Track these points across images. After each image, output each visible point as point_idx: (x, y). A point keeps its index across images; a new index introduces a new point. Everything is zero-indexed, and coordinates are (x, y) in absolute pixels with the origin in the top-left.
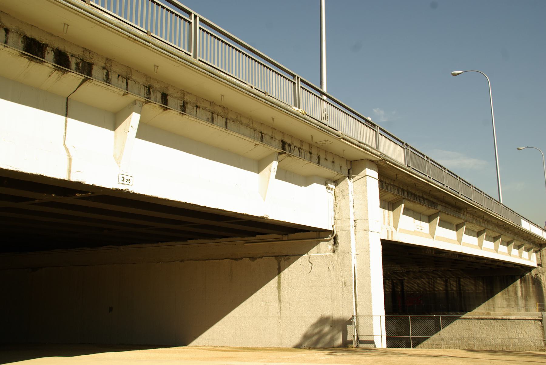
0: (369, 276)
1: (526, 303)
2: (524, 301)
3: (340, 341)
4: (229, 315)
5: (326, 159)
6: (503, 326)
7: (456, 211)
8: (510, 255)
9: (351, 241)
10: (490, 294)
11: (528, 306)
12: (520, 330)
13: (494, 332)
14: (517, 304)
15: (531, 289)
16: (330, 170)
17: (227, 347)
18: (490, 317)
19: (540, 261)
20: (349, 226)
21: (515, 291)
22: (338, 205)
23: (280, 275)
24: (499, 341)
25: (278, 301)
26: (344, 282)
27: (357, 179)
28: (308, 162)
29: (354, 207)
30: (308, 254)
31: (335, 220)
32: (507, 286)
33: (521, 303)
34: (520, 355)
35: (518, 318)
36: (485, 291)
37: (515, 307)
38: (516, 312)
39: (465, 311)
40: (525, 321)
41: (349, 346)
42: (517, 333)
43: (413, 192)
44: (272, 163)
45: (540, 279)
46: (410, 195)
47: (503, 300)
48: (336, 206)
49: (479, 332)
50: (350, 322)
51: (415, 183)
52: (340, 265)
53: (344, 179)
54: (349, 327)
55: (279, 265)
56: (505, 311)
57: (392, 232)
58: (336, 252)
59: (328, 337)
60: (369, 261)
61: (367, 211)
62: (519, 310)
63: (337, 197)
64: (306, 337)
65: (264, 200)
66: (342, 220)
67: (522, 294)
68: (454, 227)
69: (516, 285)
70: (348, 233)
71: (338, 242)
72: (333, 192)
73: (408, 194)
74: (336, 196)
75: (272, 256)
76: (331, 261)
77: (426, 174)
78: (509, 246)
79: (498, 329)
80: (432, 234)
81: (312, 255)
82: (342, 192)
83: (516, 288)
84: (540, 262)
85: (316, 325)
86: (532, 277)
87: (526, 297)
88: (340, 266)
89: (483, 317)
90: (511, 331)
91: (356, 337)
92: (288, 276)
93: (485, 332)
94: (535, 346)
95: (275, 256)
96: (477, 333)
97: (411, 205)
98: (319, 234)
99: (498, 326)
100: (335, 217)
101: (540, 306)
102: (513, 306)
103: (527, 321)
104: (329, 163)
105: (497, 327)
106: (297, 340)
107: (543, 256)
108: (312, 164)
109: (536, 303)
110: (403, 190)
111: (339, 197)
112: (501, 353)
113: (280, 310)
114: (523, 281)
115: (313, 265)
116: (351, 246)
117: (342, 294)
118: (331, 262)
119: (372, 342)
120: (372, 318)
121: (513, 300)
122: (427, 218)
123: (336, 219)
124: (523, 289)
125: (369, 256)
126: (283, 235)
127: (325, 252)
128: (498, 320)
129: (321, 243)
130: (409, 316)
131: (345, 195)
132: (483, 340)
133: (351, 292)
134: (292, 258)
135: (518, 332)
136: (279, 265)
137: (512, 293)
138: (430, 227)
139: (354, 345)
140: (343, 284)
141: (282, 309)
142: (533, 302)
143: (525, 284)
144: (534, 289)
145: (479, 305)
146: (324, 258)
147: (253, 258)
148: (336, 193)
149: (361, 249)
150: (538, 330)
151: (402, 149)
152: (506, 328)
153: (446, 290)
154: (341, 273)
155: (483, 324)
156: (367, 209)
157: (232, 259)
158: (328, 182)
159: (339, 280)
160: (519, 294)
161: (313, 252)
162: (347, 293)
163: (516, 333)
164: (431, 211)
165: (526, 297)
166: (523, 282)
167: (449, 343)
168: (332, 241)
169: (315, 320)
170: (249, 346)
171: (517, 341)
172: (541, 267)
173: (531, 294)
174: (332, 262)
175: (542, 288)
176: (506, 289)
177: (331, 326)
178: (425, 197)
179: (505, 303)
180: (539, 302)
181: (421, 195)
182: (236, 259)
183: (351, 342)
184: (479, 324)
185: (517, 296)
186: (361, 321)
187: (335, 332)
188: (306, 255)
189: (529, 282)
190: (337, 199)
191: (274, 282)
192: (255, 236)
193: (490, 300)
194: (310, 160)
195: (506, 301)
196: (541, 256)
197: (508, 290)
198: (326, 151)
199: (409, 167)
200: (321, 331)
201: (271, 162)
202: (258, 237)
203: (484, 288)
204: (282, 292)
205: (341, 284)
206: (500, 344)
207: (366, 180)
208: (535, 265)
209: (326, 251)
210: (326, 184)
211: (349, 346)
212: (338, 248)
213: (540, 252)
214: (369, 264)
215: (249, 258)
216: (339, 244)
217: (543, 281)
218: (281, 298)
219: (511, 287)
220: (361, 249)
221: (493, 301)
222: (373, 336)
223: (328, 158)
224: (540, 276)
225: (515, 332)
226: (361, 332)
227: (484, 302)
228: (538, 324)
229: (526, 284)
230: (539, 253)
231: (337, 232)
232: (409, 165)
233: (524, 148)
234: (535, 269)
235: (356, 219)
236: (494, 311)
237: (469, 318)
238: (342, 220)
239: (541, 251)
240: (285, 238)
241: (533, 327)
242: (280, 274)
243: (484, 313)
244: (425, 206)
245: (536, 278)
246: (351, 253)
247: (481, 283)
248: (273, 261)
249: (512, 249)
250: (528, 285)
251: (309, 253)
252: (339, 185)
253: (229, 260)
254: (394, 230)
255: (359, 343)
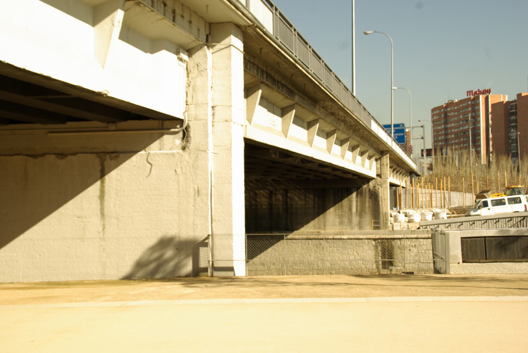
0: (230, 183)
1: (360, 219)
2: (358, 218)
3: (189, 268)
4: (22, 237)
5: (182, 16)
6: (334, 247)
7: (312, 105)
8: (354, 163)
9: (208, 134)
10: (321, 210)
11: (363, 223)
12: (351, 251)
13: (324, 254)
14: (350, 221)
15: (367, 204)
16: (186, 33)
17: (18, 283)
18: (320, 237)
19: (380, 171)
20: (207, 114)
21: (349, 206)
22: (192, 84)
23: (104, 180)
24: (328, 264)
25: (100, 215)
26: (196, 189)
27: (218, 50)
28: (161, 17)
29: (212, 88)
30: (145, 151)
31: (187, 104)
32: (341, 199)
33: (355, 219)
34: (482, 280)
35: (351, 237)
36: (316, 206)
37: (348, 224)
38: (349, 231)
39: (291, 229)
40: (358, 240)
41: (202, 275)
42: (348, 254)
43: (273, 75)
44: (116, 12)
45: (378, 191)
46: (269, 79)
47: (336, 216)
48: (189, 86)
49: (307, 255)
50: (204, 243)
51: (278, 63)
52: (191, 166)
53: (200, 47)
54: (202, 250)
55: (102, 165)
56: (337, 229)
57: (246, 126)
58: (187, 149)
59: (172, 264)
60: (231, 162)
61: (231, 94)
62: (352, 228)
63: (190, 73)
64: (140, 265)
65: (103, 67)
66: (197, 105)
67: (357, 209)
68: (306, 125)
69: (352, 199)
70: (204, 123)
71: (190, 135)
72: (184, 65)
73: (267, 77)
74: (189, 71)
75: (92, 153)
76: (180, 162)
77: (293, 51)
78: (355, 152)
79: (328, 250)
80: (285, 132)
81: (152, 152)
82: (198, 66)
83: (350, 203)
84: (379, 173)
85: (153, 249)
86: (370, 189)
87: (361, 213)
88: (192, 168)
89: (312, 237)
90: (342, 253)
91: (211, 263)
92: (116, 180)
93: (313, 254)
94: (367, 269)
95: (97, 153)
96: (303, 256)
97: (268, 91)
98: (163, 123)
99: (328, 247)
100: (187, 101)
101: (375, 223)
102: (346, 224)
103: (360, 240)
104: (186, 23)
105: (327, 248)
106: (126, 268)
107: (383, 165)
108: (165, 21)
109: (372, 220)
110: (262, 71)
111: (193, 74)
112: (258, 278)
113: (104, 229)
114: (360, 194)
115: (153, 166)
116: (208, 141)
117: (193, 206)
118: (179, 163)
119: (231, 269)
120: (232, 238)
121: (347, 216)
122: (279, 111)
123: (188, 103)
124: (359, 204)
125: (231, 156)
126: (108, 122)
127: (171, 149)
128: (328, 240)
129: (166, 137)
130: (283, 235)
131: (202, 71)
132: (310, 263)
133: (207, 204)
134: (122, 155)
135: (349, 253)
136: (102, 165)
137: (346, 209)
138: (283, 123)
139: (209, 273)
140: (195, 193)
141: (106, 226)
142: (368, 219)
143: (361, 198)
144: (371, 204)
145: (307, 222)
146: (169, 157)
147: (62, 155)
148: (189, 67)
149: (221, 146)
150: (371, 251)
151: (271, 14)
152: (337, 250)
153: (271, 205)
154: (192, 177)
155: (312, 244)
156: (231, 92)
157: (28, 155)
158: (181, 50)
159: (190, 188)
160: (354, 210)
161: (154, 148)
162: (200, 205)
163: (347, 254)
164: (287, 102)
165: (361, 213)
166: (359, 195)
167: (271, 269)
168: (181, 134)
169: (152, 241)
170: (54, 279)
171: (347, 263)
172: (381, 177)
173: (367, 210)
174: (181, 163)
175: (378, 203)
176: (340, 204)
177: (177, 249)
178: (283, 82)
179: (337, 220)
180: (375, 219)
181: (280, 80)
182: (34, 156)
183: (205, 270)
184: (307, 245)
185: (351, 212)
186: (217, 241)
187: (182, 257)
188: (143, 152)
189: (365, 196)
190: (190, 76)
191: (94, 189)
192: (64, 122)
193: (321, 216)
194: (164, 15)
195: (339, 218)
196: (382, 166)
197: (342, 206)
198: (183, 5)
199: (277, 39)
200: (158, 258)
201: (114, 10)
202: (69, 124)
203: (314, 201)
204: (106, 204)
205: (193, 193)
206: (329, 267)
207: (230, 51)
208: (374, 175)
209: (173, 147)
210: (177, 53)
211: (201, 274)
212: (190, 143)
213: (381, 160)
214: (231, 166)
215: (56, 154)
216: (192, 138)
217: (381, 195)
218: (106, 212)
219: (345, 202)
220: (221, 146)
221: (325, 218)
222: (233, 260)
223: (184, 16)
224: (379, 188)
225: (346, 254)
226: (217, 256)
227: (313, 219)
228: (372, 244)
229: (363, 198)
230: (379, 162)
231: (189, 122)
232: (277, 37)
233: (371, 32)
234: (373, 181)
235: (214, 105)
236: (324, 229)
237: (295, 238)
238: (197, 105)
239: (382, 159)
240: (112, 127)
241: (366, 247)
242: (104, 178)
243: (313, 232)
244: (282, 95)
245: (374, 191)
246: (208, 151)
247: (312, 197)
248: (95, 161)
249: (356, 156)
250: (364, 199)
251: (147, 149)
252: (194, 56)
253: (22, 156)
254: (247, 123)
255: (213, 271)
